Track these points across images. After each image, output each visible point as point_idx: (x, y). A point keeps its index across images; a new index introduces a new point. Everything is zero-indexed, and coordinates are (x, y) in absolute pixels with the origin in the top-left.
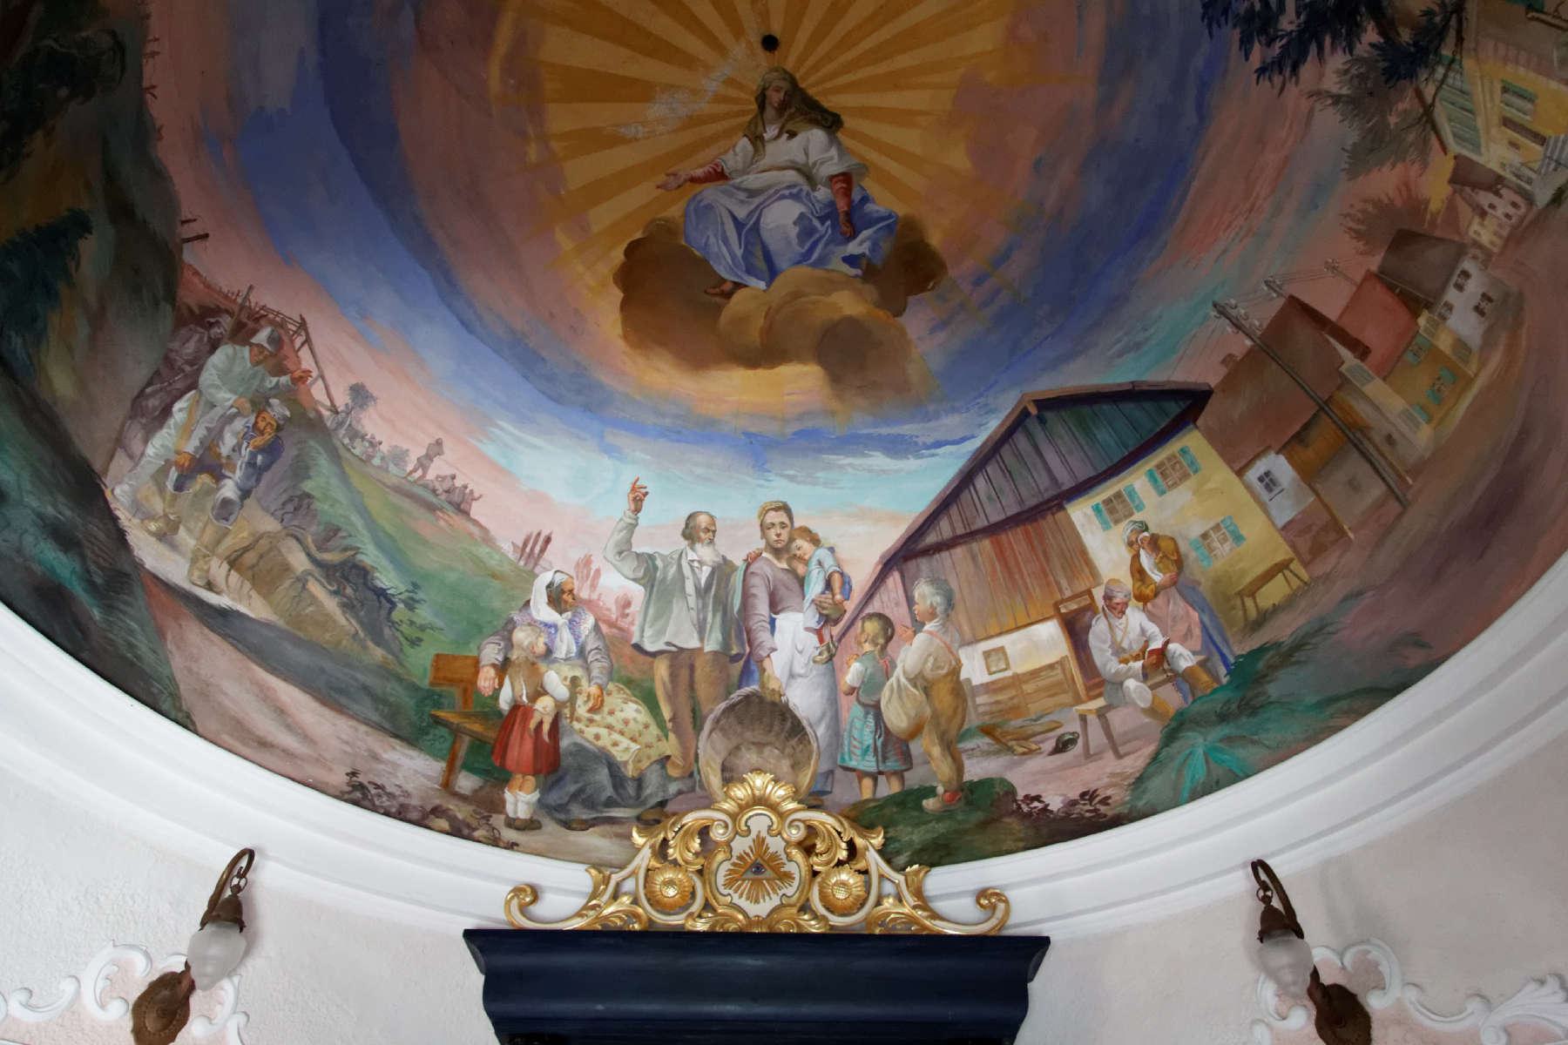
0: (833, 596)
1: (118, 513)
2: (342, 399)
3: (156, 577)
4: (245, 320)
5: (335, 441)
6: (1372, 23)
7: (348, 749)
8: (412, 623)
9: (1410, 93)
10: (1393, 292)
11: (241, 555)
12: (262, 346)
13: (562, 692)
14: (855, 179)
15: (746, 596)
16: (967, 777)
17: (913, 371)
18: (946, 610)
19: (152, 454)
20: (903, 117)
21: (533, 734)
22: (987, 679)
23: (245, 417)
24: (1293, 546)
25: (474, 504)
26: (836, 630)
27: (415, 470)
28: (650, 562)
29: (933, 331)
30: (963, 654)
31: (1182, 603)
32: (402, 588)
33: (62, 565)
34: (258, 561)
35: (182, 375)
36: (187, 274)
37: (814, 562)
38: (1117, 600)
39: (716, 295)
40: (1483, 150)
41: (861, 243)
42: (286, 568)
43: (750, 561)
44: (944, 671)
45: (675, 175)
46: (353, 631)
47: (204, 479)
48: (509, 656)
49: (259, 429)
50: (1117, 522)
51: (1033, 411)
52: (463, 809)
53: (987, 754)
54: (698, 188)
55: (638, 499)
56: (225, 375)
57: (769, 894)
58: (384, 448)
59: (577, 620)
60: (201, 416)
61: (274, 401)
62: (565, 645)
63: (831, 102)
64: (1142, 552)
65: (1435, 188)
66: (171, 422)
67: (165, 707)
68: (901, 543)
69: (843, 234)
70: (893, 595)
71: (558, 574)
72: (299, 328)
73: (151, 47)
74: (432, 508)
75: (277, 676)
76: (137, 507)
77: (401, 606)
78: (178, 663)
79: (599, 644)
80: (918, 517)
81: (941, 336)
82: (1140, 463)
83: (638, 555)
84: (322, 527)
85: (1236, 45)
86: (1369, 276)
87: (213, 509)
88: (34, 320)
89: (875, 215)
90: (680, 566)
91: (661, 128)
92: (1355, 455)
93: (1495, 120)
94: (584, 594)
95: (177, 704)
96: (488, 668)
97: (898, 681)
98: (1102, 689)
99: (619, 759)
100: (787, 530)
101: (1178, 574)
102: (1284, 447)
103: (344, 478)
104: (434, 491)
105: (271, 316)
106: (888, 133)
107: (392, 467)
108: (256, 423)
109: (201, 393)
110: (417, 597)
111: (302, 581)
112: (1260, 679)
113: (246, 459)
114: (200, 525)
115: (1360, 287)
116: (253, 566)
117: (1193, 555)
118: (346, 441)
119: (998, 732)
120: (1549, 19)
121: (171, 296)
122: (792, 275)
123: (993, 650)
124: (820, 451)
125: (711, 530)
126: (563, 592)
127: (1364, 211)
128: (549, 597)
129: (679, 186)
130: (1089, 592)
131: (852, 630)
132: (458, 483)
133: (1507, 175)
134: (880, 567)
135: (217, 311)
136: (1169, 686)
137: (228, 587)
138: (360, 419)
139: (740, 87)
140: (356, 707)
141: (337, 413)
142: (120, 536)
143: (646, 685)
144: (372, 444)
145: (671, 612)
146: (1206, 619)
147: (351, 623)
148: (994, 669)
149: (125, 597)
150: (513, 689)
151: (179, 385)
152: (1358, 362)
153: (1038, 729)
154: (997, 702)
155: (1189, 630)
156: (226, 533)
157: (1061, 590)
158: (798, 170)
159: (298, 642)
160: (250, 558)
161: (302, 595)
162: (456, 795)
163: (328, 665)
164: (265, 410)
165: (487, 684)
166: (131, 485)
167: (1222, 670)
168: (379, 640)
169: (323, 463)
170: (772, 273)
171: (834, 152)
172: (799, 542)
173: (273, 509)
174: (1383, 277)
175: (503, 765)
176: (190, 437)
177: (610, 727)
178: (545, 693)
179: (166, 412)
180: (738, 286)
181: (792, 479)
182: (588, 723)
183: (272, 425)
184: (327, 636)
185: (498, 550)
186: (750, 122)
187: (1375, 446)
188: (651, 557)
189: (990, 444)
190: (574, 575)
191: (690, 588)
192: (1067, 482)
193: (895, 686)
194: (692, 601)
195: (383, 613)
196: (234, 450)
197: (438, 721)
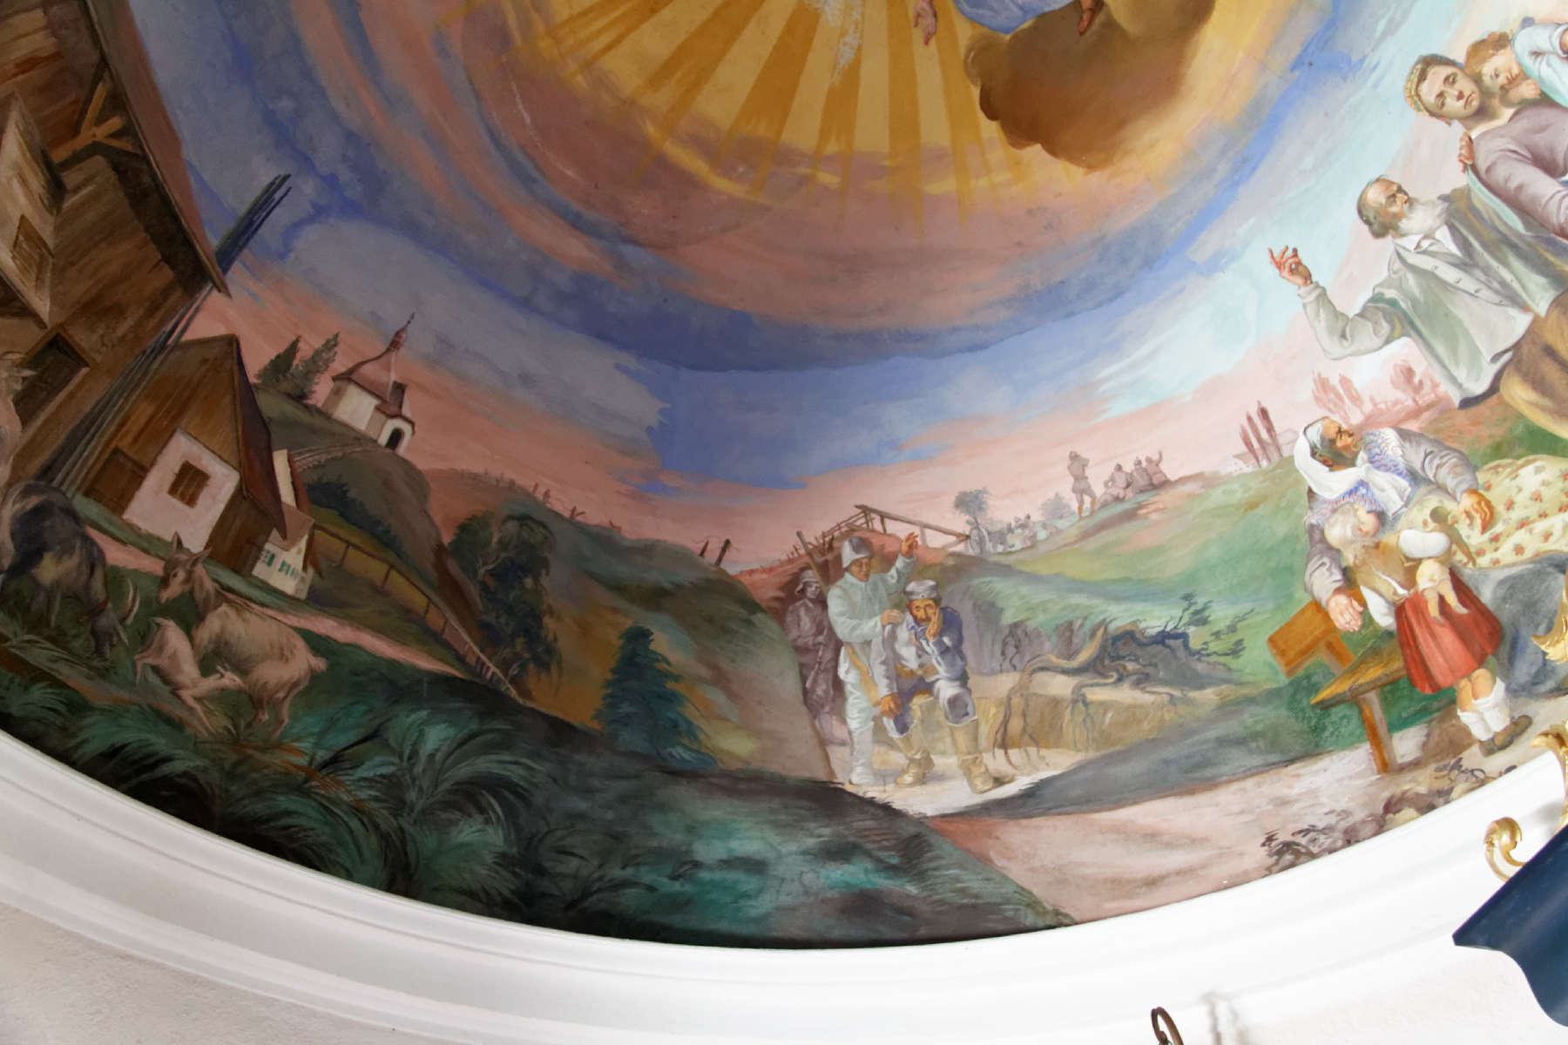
1: (869, 795)
2: (960, 523)
3: (944, 816)
4: (823, 559)
7: (1249, 818)
8: (1217, 634)
11: (1005, 730)
12: (857, 560)
13: (1436, 541)
15: (1513, 200)
19: (857, 726)
23: (901, 623)
25: (1164, 467)
27: (1081, 503)
28: (1380, 305)
32: (1177, 612)
33: (855, 874)
34: (1025, 721)
35: (822, 647)
36: (746, 580)
37: (1528, 62)
42: (1055, 702)
45: (919, 15)
46: (1166, 698)
47: (918, 702)
48: (1344, 565)
49: (923, 620)
52: (1421, 779)
55: (1294, 267)
56: (853, 612)
59: (1377, 450)
60: (868, 659)
61: (911, 587)
62: (1389, 490)
66: (849, 688)
67: (1030, 920)
71: (1309, 431)
72: (866, 516)
73: (540, 496)
74: (1130, 515)
76: (882, 777)
77: (1191, 630)
78: (1017, 872)
79: (1426, 447)
83: (1361, 315)
84: (1054, 638)
87: (947, 718)
88: (675, 725)
90: (1413, 269)
91: (856, 16)
94: (1356, 418)
95: (1041, 910)
96: (1334, 599)
100: (1460, 77)
103: (1033, 578)
104: (1117, 499)
105: (837, 534)
107: (1061, 524)
108: (915, 618)
109: (849, 644)
110: (1199, 607)
111: (1079, 699)
113: (936, 652)
114: (948, 740)
116: (1024, 729)
118: (1000, 548)
121: (752, 606)
125: (1396, 192)
126: (1333, 441)
128: (1325, 463)
129: (935, 15)
132: (1129, 467)
135: (796, 578)
137: (1015, 767)
138: (991, 519)
140: (1225, 769)
141: (968, 537)
142: (887, 808)
143: (1520, 430)
144: (1023, 526)
145: (1460, 322)
147: (1160, 694)
149: (929, 854)
150: (1381, 595)
151: (828, 656)
156: (976, 724)
159: (1123, 756)
160: (1016, 725)
161: (1090, 711)
162: (1403, 769)
163: (1169, 752)
164: (911, 601)
165: (1348, 617)
166: (862, 765)
168: (1199, 683)
169: (1000, 586)
172: (1487, 69)
173: (998, 667)
175: (1436, 688)
177: (1522, 524)
178: (1419, 561)
179: (838, 685)
181: (1392, 29)
182: (1494, 545)
183: (929, 605)
184: (1146, 726)
185: (1229, 479)
188: (1377, 299)
191: (1450, 274)
194: (1468, 283)
195: (1181, 653)
196: (920, 656)
197: (1326, 706)
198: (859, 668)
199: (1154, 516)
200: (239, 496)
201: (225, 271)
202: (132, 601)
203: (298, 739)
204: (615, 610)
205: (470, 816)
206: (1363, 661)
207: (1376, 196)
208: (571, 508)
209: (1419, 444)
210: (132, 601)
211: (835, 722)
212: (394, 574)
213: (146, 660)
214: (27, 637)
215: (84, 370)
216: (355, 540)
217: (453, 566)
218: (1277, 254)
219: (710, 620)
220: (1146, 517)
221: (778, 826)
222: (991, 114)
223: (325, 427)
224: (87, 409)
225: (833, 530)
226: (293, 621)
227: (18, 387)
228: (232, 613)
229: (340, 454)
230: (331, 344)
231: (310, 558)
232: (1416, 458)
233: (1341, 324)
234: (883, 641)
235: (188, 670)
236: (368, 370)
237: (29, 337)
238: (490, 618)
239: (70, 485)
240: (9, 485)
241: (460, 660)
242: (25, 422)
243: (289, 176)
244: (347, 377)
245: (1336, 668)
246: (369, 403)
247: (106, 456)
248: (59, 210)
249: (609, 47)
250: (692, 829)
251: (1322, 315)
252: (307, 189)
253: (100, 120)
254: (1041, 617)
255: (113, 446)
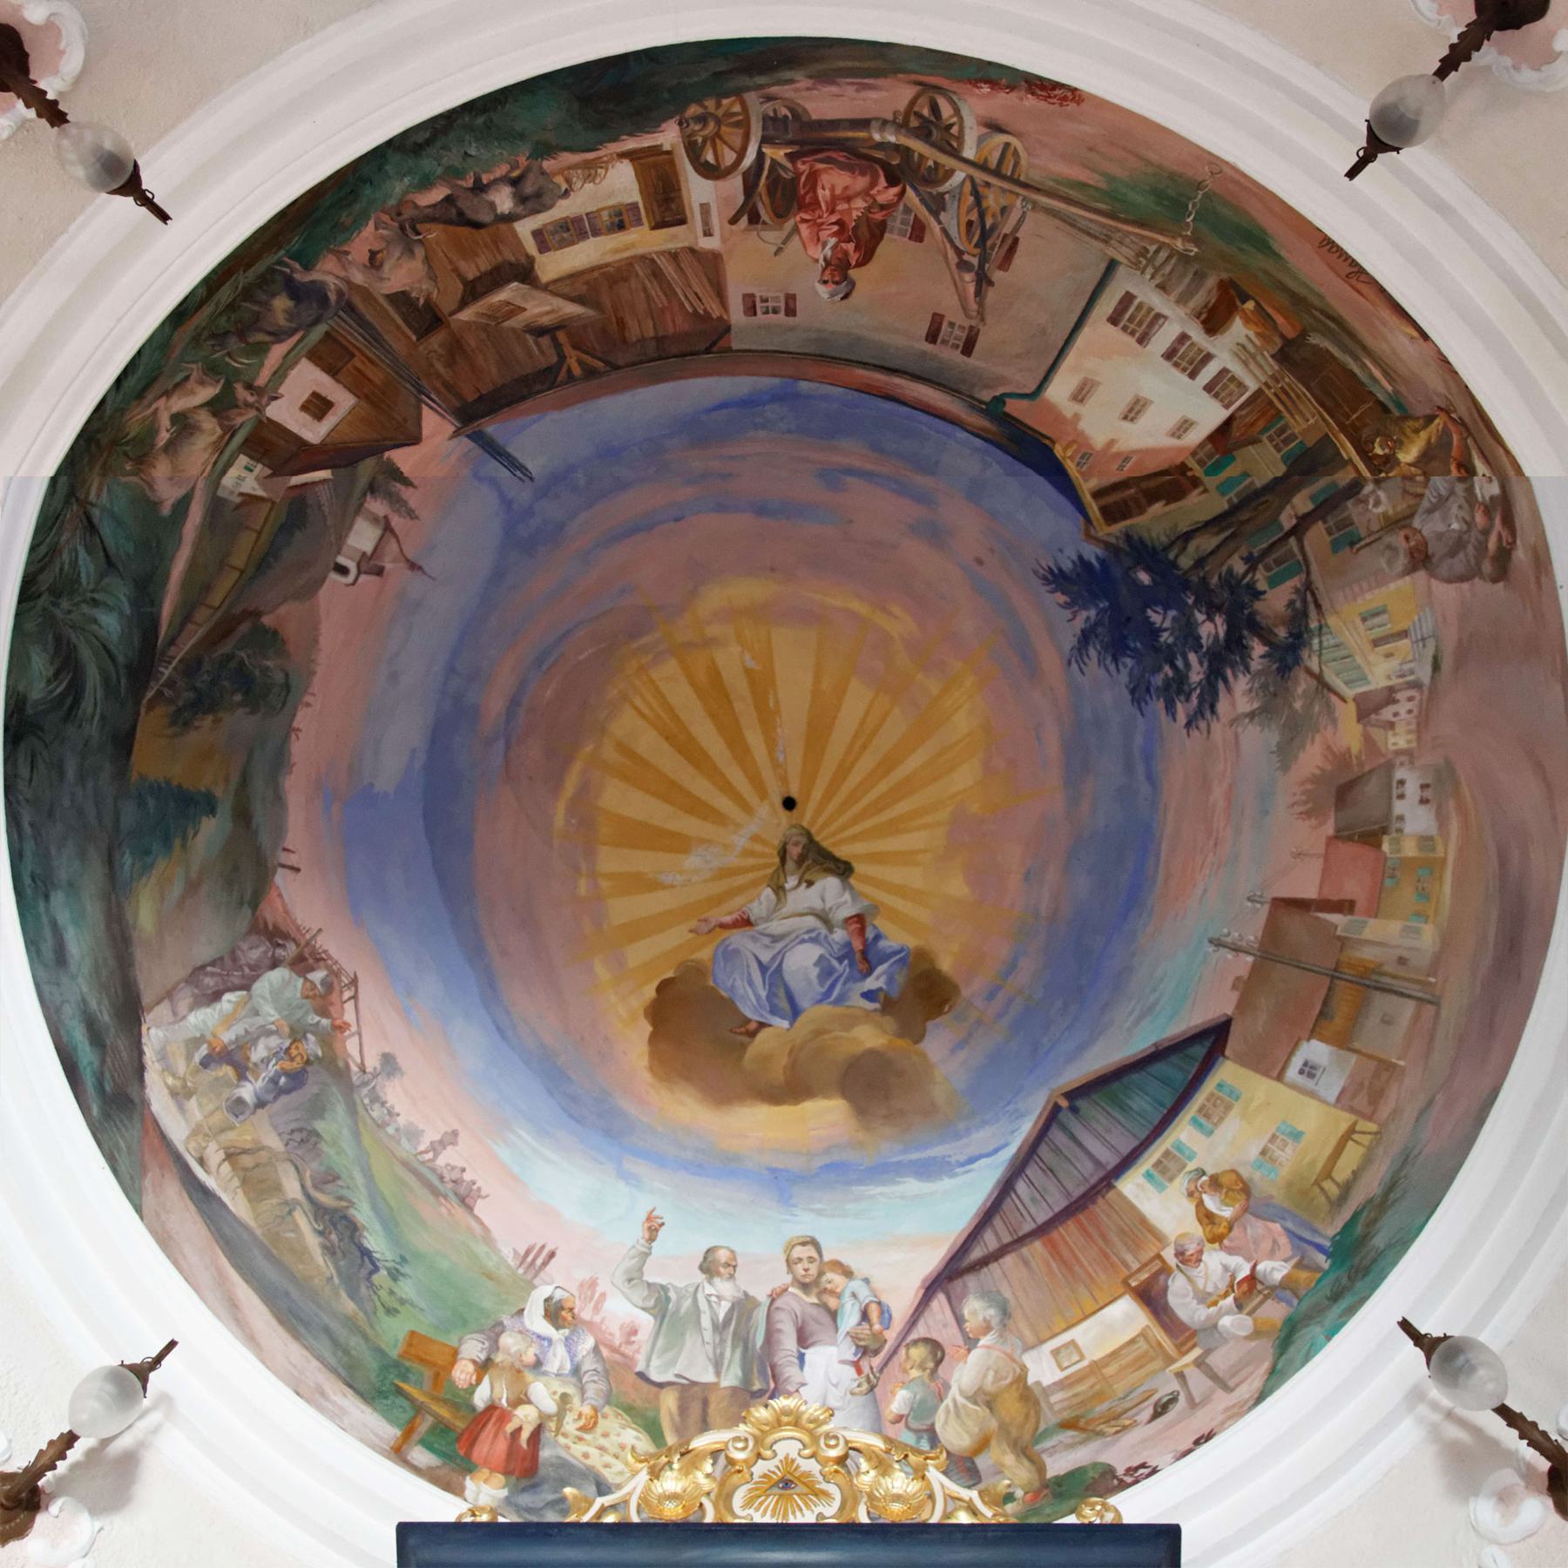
0: (871, 1326)
1: (146, 1049)
2: (372, 1063)
5: (356, 1097)
6: (1256, 639)
8: (392, 1293)
9: (1302, 676)
10: (1352, 840)
13: (550, 1406)
14: (868, 920)
16: (1050, 1474)
17: (939, 1093)
18: (1002, 1321)
20: (905, 858)
21: (508, 1435)
22: (1060, 1375)
24: (1352, 1110)
26: (877, 1361)
27: (426, 1152)
29: (953, 1051)
30: (1028, 1359)
31: (1260, 1223)
36: (274, 894)
37: (847, 1294)
38: (1188, 1253)
39: (741, 1034)
40: (1370, 677)
41: (878, 978)
42: (278, 1188)
43: (773, 1297)
44: (1009, 1380)
45: (706, 920)
46: (328, 1274)
47: (227, 1071)
50: (1171, 1180)
51: (1064, 1103)
53: (1071, 1446)
54: (726, 933)
55: (653, 1229)
56: (276, 995)
57: (801, 1510)
58: (401, 1121)
63: (842, 852)
64: (1204, 1196)
65: (1348, 733)
66: (218, 1006)
68: (944, 1263)
69: (860, 971)
70: (940, 1317)
71: (558, 1290)
73: (307, 698)
74: (436, 1193)
75: (240, 1274)
76: (163, 1056)
77: (384, 1272)
80: (960, 1234)
81: (962, 1055)
82: (1180, 1115)
83: (649, 1285)
84: (323, 1169)
85: (1163, 712)
86: (1331, 840)
88: (147, 852)
89: (889, 951)
91: (694, 879)
92: (1377, 995)
93: (1368, 647)
94: (586, 1315)
97: (955, 1401)
98: (1195, 1340)
99: (610, 1480)
101: (1248, 1200)
102: (1312, 1031)
103: (357, 1135)
104: (441, 1178)
106: (894, 874)
107: (404, 1141)
108: (289, 1048)
109: (250, 997)
110: (402, 1270)
111: (290, 1206)
112: (1365, 1239)
115: (1326, 858)
117: (1257, 1176)
118: (366, 1101)
119: (1082, 1423)
120: (1368, 541)
121: (255, 906)
122: (814, 1013)
123: (1063, 1346)
124: (849, 1183)
125: (732, 1265)
126: (562, 1308)
127: (1303, 793)
130: (1159, 1256)
131: (895, 1359)
132: (467, 1177)
133: (1395, 681)
134: (922, 1291)
135: (286, 936)
136: (1269, 1302)
137: (218, 1172)
139: (763, 842)
141: (364, 1072)
142: (141, 1069)
143: (650, 1414)
144: (390, 1113)
146: (1290, 1225)
148: (1066, 1364)
151: (236, 981)
152: (1349, 917)
153: (1129, 1405)
154: (1075, 1395)
155: (1275, 1242)
156: (232, 1128)
157: (1126, 1266)
158: (817, 916)
159: (269, 1255)
160: (247, 1161)
164: (300, 1041)
167: (1321, 1259)
170: (795, 1012)
171: (847, 896)
172: (829, 1275)
174: (1340, 836)
175: (468, 1455)
176: (228, 1029)
177: (601, 1448)
178: (529, 1402)
179: (216, 996)
180: (762, 1025)
181: (819, 1212)
185: (497, 1251)
186: (772, 876)
187: (1394, 977)
188: (664, 1288)
189: (1026, 1149)
190: (576, 1293)
191: (706, 1322)
192: (1110, 1160)
193: (952, 1408)
194: (708, 1335)
197: (400, 1392)
198: (235, 1010)
199: (443, 1210)
200: (301, 443)
201: (469, 436)
202: (241, 363)
203: (109, 491)
204: (227, 780)
205: (52, 663)
206: (445, 1402)
207: (723, 1255)
208: (1195, 733)
209: (598, 1361)
210: (241, 363)
211: (189, 1000)
212: (236, 574)
213: (196, 370)
214: (240, 287)
215: (414, 338)
216: (264, 537)
217: (244, 628)
218: (655, 1213)
219: (236, 868)
220: (441, 1204)
221: (96, 969)
222: (659, 989)
223: (349, 511)
224: (386, 337)
225: (330, 957)
226: (200, 484)
227: (413, 295)
228: (214, 438)
229: (329, 523)
230: (411, 514)
231: (250, 499)
232: (589, 1365)
233: (635, 1275)
234: (264, 1026)
235: (179, 403)
236: (393, 546)
237: (445, 304)
238: (206, 666)
239: (337, 323)
240: (348, 282)
241: (172, 641)
242: (388, 297)
243: (531, 479)
244: (388, 528)
245: (427, 1384)
246: (368, 547)
247: (351, 348)
248: (525, 332)
249: (637, 709)
250: (72, 887)
251: (634, 1261)
252: (522, 494)
253: (580, 362)
254: (331, 1152)
255: (357, 353)
